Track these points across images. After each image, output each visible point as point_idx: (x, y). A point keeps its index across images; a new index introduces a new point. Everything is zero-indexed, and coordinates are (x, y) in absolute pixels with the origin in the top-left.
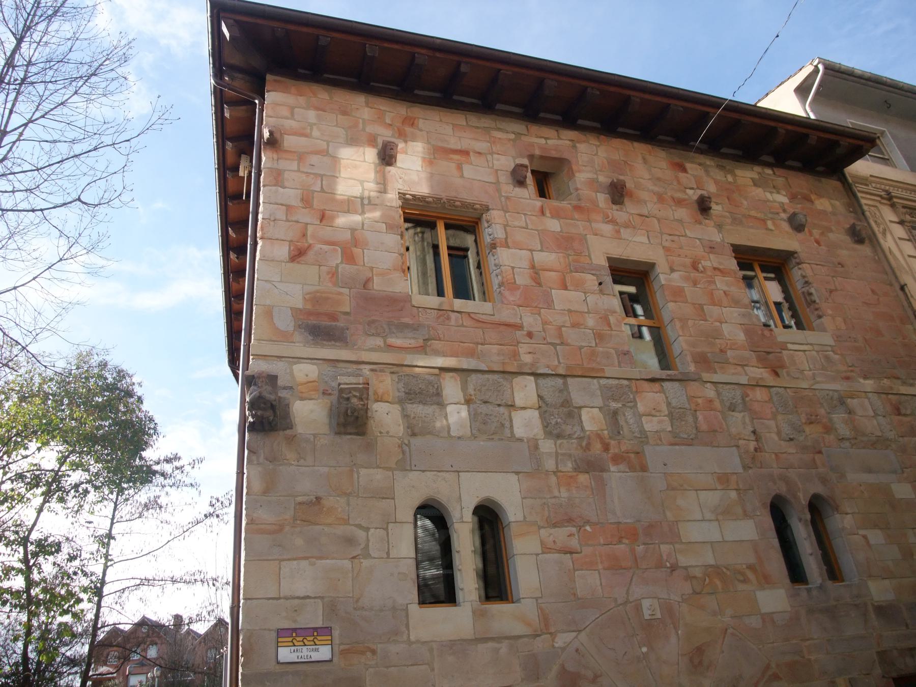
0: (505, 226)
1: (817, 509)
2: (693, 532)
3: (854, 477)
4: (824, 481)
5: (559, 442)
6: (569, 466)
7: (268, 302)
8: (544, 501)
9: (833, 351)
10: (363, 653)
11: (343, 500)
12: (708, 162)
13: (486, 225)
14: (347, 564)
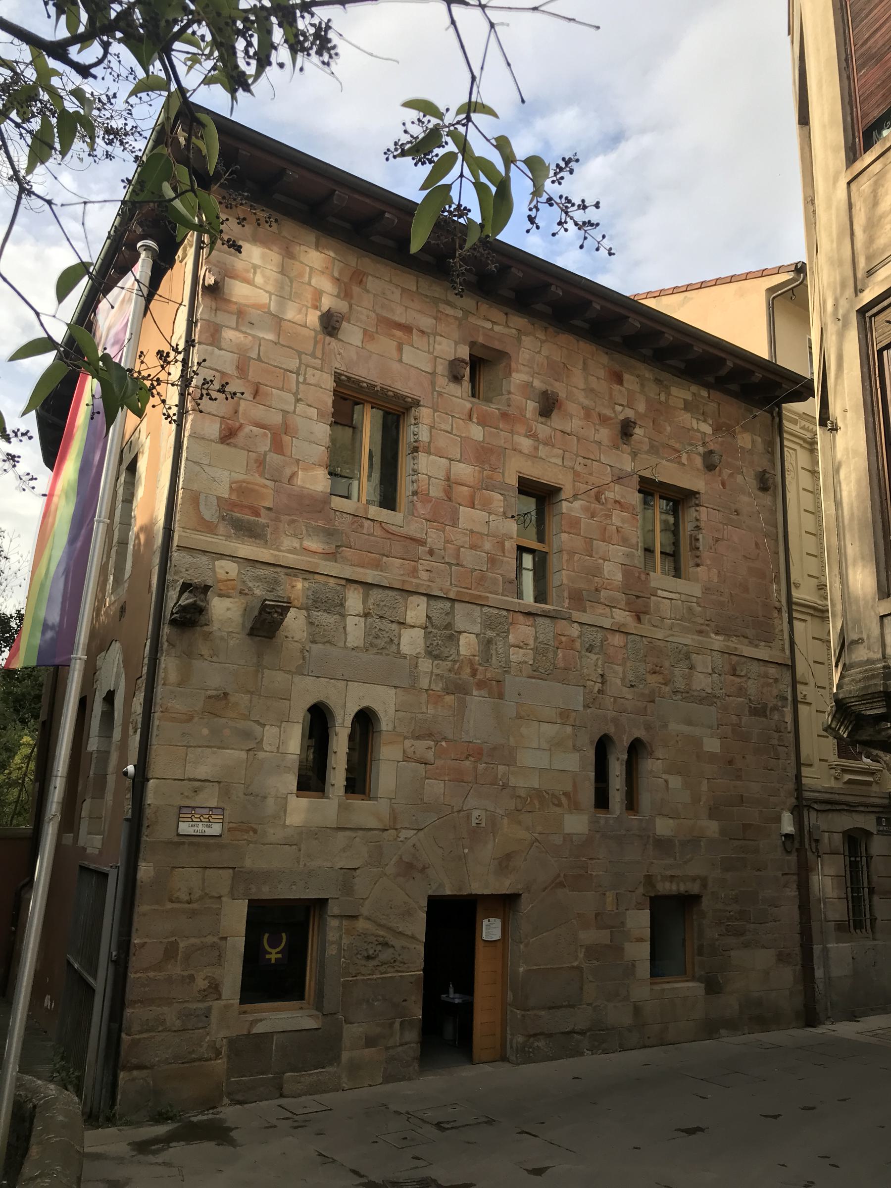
0: (432, 428)
1: (636, 749)
2: (527, 758)
3: (674, 727)
4: (648, 728)
5: (436, 662)
6: (438, 687)
7: (195, 487)
8: (413, 715)
9: (697, 603)
10: (247, 832)
11: (247, 697)
12: (648, 375)
13: (413, 421)
14: (243, 755)
